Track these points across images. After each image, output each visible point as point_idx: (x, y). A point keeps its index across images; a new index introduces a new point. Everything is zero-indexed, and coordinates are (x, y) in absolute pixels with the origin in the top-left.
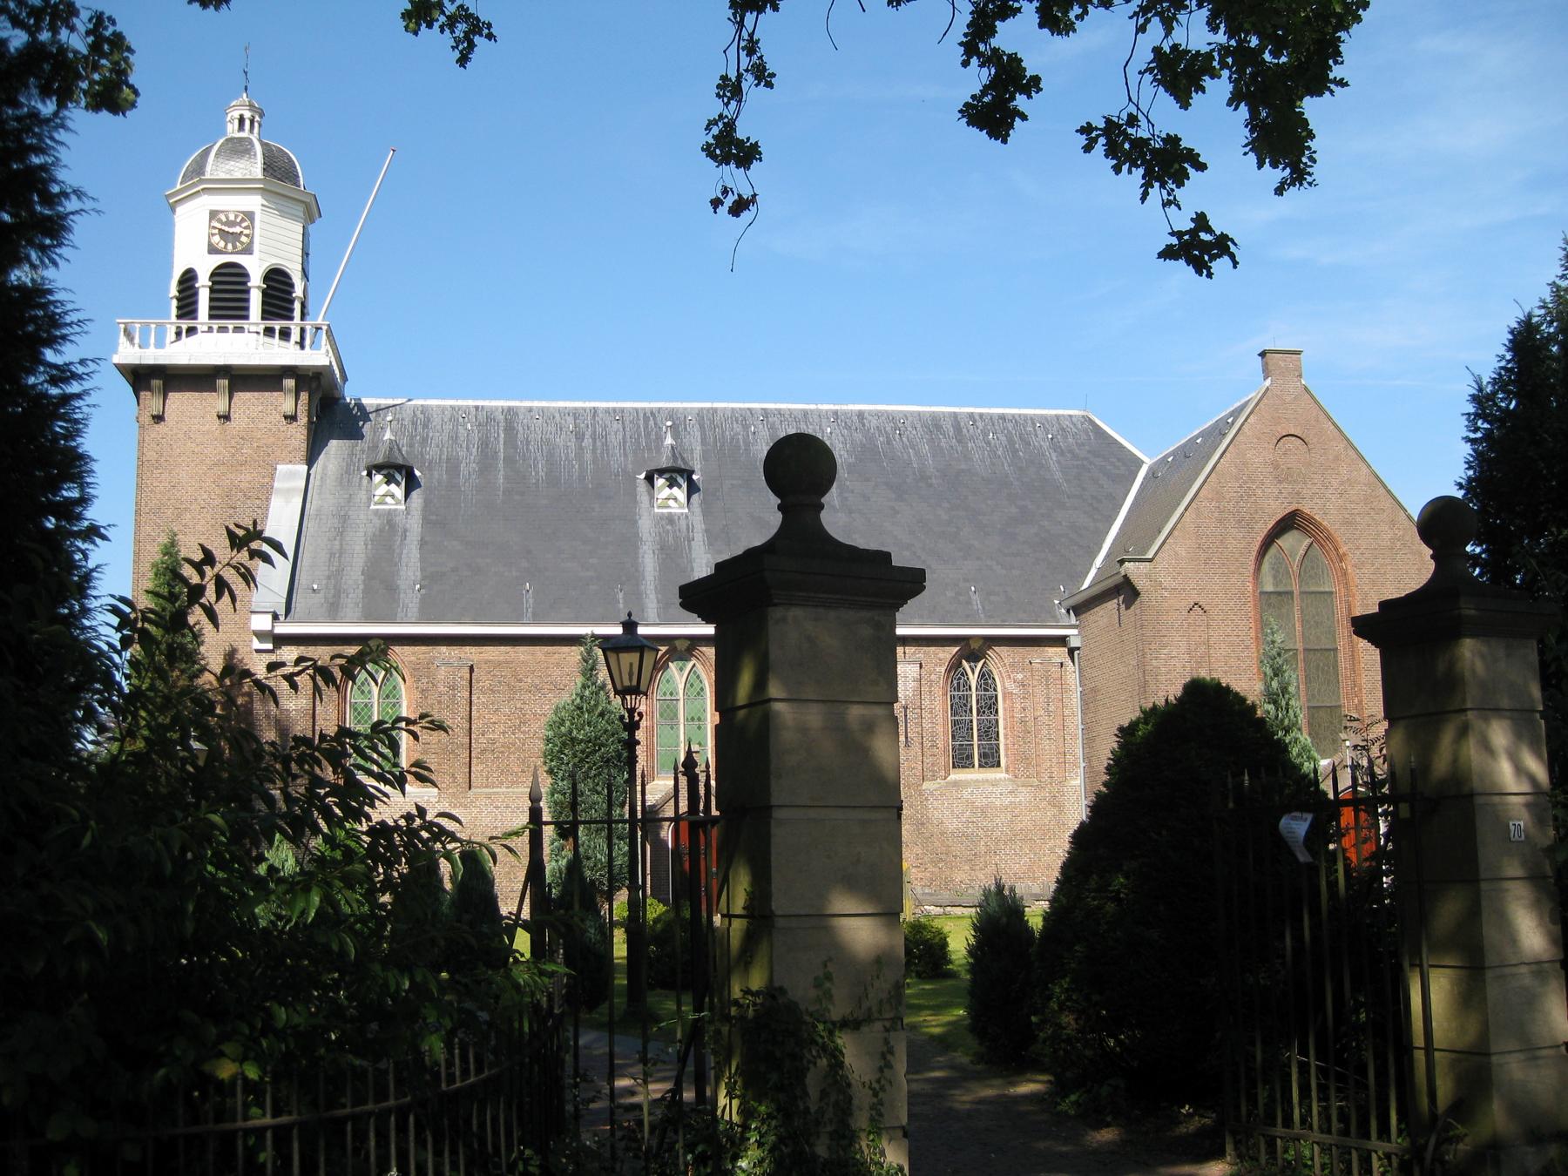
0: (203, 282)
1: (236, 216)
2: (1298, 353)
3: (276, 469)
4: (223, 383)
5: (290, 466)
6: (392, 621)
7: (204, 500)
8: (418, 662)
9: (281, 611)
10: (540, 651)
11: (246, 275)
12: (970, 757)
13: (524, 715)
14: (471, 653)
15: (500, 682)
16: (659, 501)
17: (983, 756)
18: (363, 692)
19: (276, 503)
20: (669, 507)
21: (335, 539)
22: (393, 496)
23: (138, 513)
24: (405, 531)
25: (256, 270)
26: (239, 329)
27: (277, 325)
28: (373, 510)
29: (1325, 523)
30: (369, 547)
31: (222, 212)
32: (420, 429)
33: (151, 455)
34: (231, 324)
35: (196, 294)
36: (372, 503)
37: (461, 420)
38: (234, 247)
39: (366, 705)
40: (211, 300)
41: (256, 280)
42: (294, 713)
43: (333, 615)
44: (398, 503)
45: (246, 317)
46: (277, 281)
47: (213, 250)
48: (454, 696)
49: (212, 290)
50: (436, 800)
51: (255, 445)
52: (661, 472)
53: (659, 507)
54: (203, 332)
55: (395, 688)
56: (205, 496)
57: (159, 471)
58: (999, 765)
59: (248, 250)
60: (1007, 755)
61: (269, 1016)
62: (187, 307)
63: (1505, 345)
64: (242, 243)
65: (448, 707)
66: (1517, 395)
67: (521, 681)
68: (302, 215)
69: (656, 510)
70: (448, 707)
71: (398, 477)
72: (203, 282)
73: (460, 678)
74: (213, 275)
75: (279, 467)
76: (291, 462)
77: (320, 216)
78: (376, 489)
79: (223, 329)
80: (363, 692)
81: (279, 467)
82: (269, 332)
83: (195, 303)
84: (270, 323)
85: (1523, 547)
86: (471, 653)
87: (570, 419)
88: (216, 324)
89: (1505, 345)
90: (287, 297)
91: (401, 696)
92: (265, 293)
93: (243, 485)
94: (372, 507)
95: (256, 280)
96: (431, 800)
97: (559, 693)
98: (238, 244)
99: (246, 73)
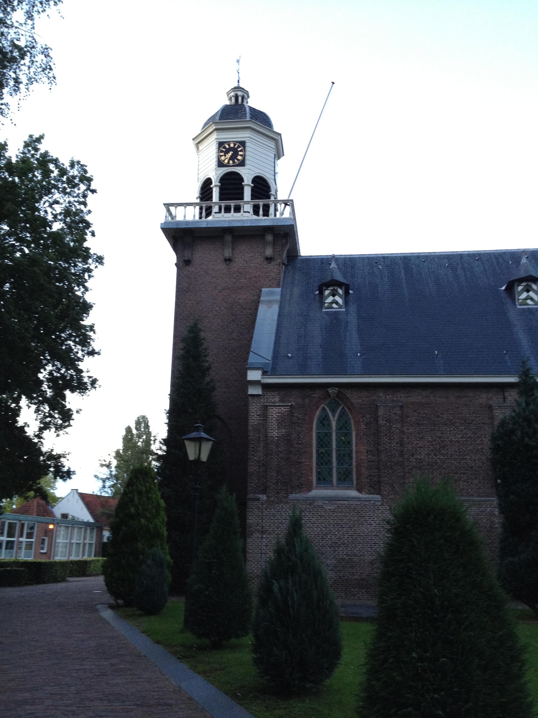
0: (215, 182)
1: (235, 145)
3: (261, 291)
4: (228, 238)
5: (270, 289)
6: (344, 373)
7: (216, 311)
8: (363, 403)
9: (269, 369)
11: (241, 179)
13: (443, 442)
14: (402, 397)
15: (422, 417)
16: (520, 301)
18: (324, 425)
19: (262, 309)
20: (527, 304)
21: (301, 328)
22: (337, 303)
24: (347, 323)
28: (324, 312)
30: (324, 332)
31: (226, 142)
32: (349, 270)
36: (324, 308)
37: (374, 264)
38: (234, 162)
39: (326, 434)
41: (248, 180)
42: (276, 438)
43: (303, 372)
44: (340, 307)
45: (242, 199)
47: (220, 164)
48: (391, 427)
50: (380, 503)
51: (248, 277)
52: (520, 281)
53: (521, 305)
54: (215, 213)
55: (346, 422)
56: (217, 309)
57: (189, 294)
59: (242, 164)
61: (46, 229)
64: (238, 160)
65: (386, 435)
67: (438, 417)
68: (273, 147)
69: (519, 307)
70: (386, 435)
73: (394, 414)
75: (263, 289)
76: (270, 286)
77: (283, 155)
78: (326, 299)
79: (228, 209)
80: (324, 425)
81: (263, 289)
84: (257, 201)
86: (401, 397)
87: (445, 261)
88: (223, 204)
90: (266, 194)
91: (351, 428)
92: (253, 190)
93: (240, 301)
94: (324, 310)
95: (248, 180)
96: (377, 503)
97: (469, 426)
98: (236, 160)
99: (238, 73)
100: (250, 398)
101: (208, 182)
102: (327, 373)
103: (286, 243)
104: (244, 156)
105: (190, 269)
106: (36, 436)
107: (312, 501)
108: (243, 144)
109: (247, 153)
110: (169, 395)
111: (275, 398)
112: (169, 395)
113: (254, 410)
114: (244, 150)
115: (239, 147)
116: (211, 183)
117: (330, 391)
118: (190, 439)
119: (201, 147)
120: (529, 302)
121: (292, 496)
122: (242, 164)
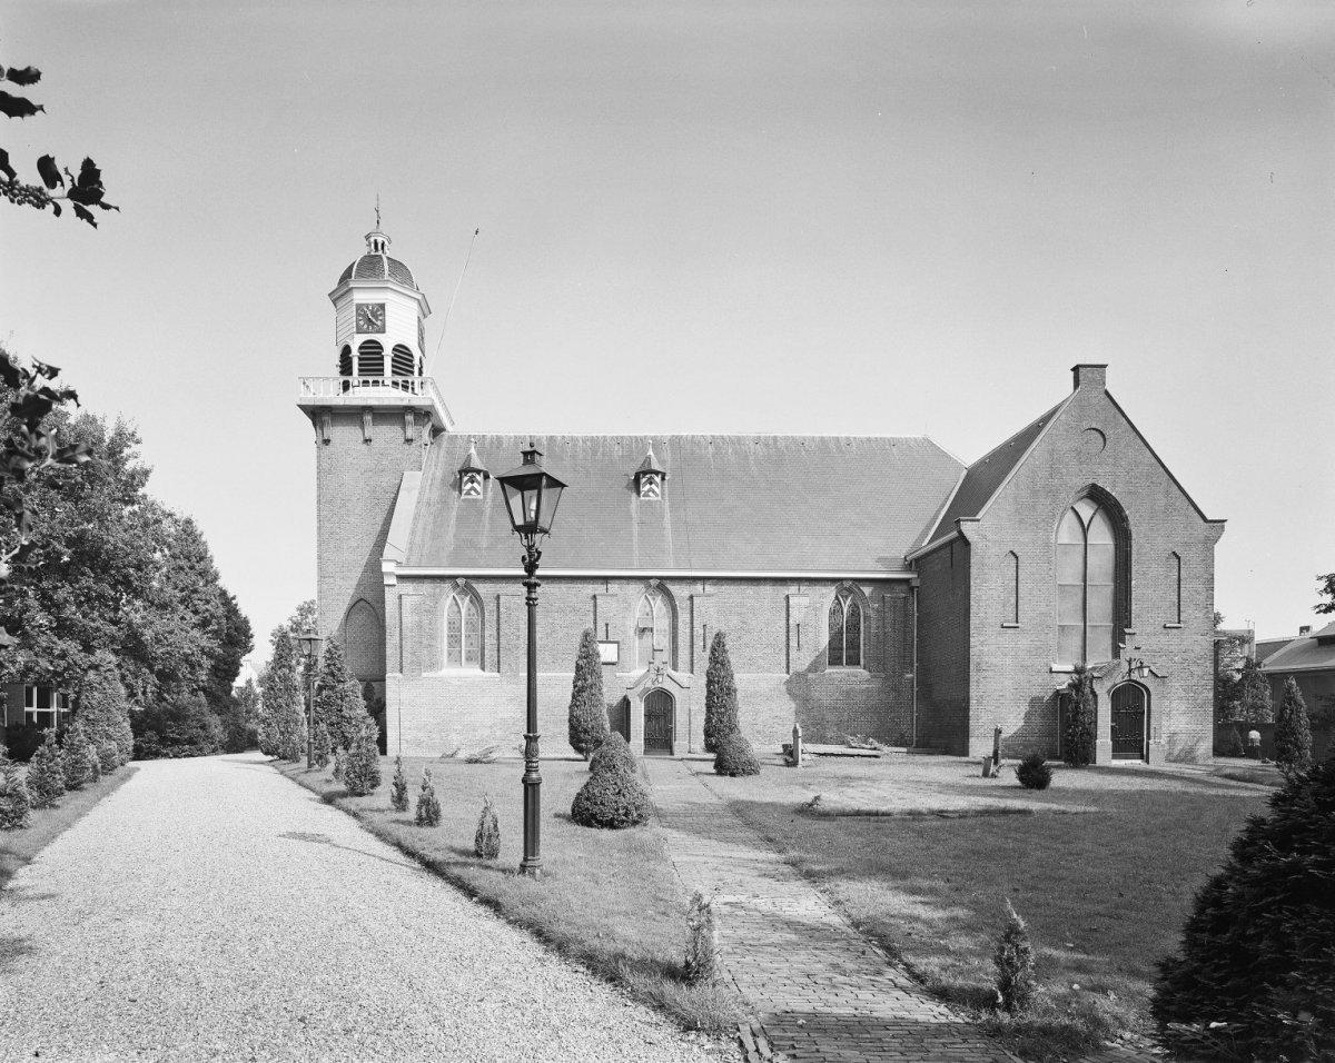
2: (1105, 366)
9: (404, 561)
10: (564, 587)
12: (841, 658)
17: (848, 657)
22: (475, 490)
23: (319, 502)
25: (388, 342)
26: (376, 383)
27: (400, 379)
29: (1113, 494)
33: (325, 465)
34: (371, 379)
35: (351, 362)
40: (360, 365)
46: (402, 354)
49: (360, 359)
58: (859, 664)
59: (382, 330)
60: (865, 658)
62: (346, 368)
63: (106, 207)
66: (22, 418)
71: (478, 477)
72: (355, 352)
74: (360, 348)
79: (366, 383)
82: (395, 384)
83: (351, 368)
84: (365, 378)
85: (901, 675)
88: (362, 379)
89: (106, 207)
100: (387, 589)
101: (347, 350)
102: (453, 565)
103: (429, 420)
104: (383, 321)
105: (327, 450)
106: (292, 630)
107: (441, 680)
108: (382, 306)
109: (387, 318)
110: (22, 116)
111: (408, 588)
112: (22, 116)
113: (390, 597)
115: (378, 310)
116: (350, 352)
117: (459, 581)
118: (80, 454)
119: (340, 304)
120: (650, 494)
121: (424, 675)
122: (382, 330)
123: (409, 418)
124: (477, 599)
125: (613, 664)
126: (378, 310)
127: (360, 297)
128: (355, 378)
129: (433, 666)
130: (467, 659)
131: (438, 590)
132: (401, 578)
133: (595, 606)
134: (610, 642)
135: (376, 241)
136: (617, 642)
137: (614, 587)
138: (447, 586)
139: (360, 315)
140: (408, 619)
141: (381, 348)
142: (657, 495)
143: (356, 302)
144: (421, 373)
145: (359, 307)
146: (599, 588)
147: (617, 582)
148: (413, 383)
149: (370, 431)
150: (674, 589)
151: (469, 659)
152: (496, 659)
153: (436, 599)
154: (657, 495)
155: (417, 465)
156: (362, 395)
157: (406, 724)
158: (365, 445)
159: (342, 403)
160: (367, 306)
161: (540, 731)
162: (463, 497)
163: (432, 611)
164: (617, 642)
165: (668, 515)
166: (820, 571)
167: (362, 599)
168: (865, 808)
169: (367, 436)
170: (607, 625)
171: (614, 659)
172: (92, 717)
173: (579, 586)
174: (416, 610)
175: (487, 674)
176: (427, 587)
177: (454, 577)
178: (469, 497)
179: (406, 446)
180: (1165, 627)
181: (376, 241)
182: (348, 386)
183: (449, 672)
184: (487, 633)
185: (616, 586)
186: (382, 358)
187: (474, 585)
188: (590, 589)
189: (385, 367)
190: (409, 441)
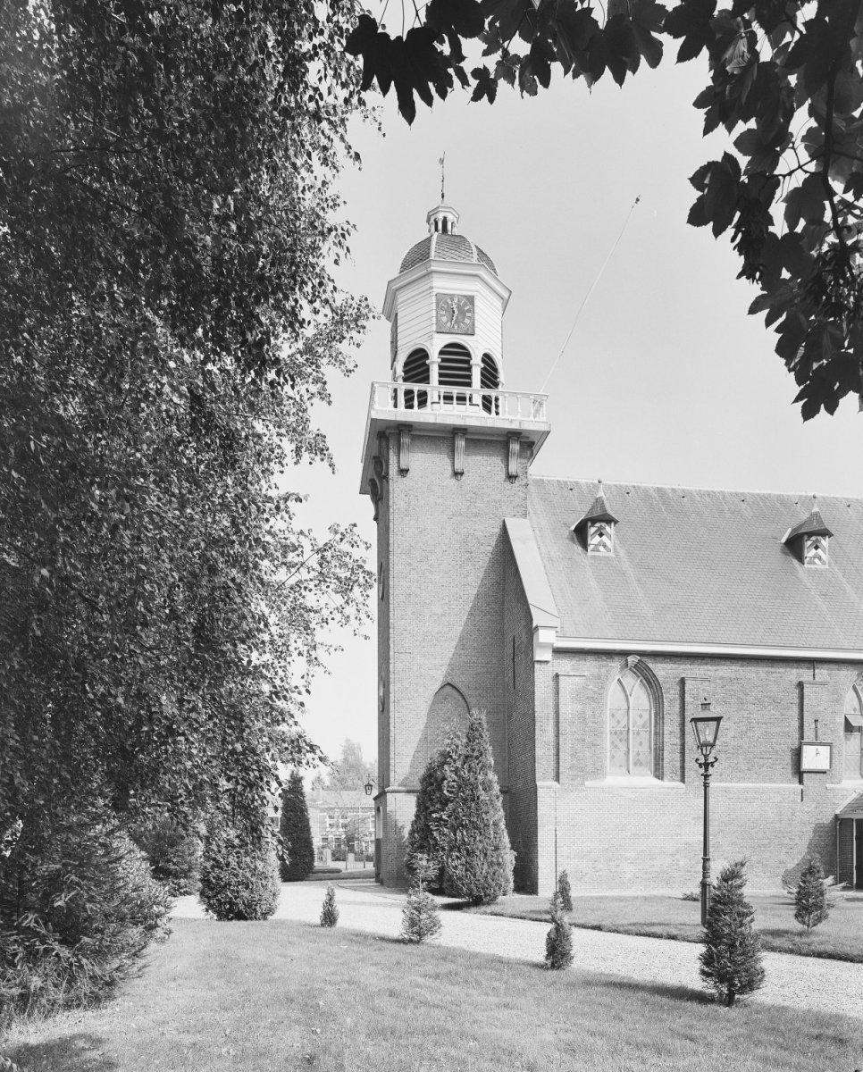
26: (461, 399)
35: (427, 370)
49: (441, 367)
74: (441, 353)
100: (537, 666)
104: (472, 319)
108: (471, 300)
109: (477, 317)
111: (565, 665)
113: (542, 678)
114: (472, 311)
115: (465, 305)
123: (461, 443)
124: (651, 683)
125: (824, 772)
126: (465, 305)
127: (441, 285)
128: (434, 388)
129: (597, 772)
130: (635, 764)
131: (603, 670)
132: (558, 652)
133: (802, 697)
134: (821, 744)
135: (445, 218)
136: (830, 745)
137: (822, 673)
138: (616, 664)
139: (442, 308)
140: (567, 709)
141: (468, 355)
142: (609, 550)
143: (436, 291)
144: (395, 391)
145: (440, 298)
146: (805, 674)
147: (825, 666)
148: (497, 399)
149: (462, 461)
150: (661, 670)
151: (638, 763)
152: (678, 765)
153: (601, 681)
154: (609, 550)
155: (521, 510)
156: (438, 413)
157: (562, 850)
158: (454, 480)
159: (432, 421)
160: (452, 297)
161: (711, 856)
162: (589, 553)
163: (597, 698)
164: (830, 745)
165: (848, 587)
166: (753, 645)
167: (449, 684)
168: (848, 964)
169: (458, 467)
170: (816, 721)
171: (826, 767)
172: (466, 840)
173: (780, 669)
174: (578, 696)
175: (666, 783)
176: (589, 666)
177: (624, 654)
178: (597, 554)
179: (508, 485)
180: (816, 721)
181: (445, 218)
182: (425, 401)
183: (614, 779)
184: (667, 729)
185: (825, 672)
186: (469, 369)
187: (650, 665)
188: (794, 674)
189: (474, 381)
190: (511, 478)
